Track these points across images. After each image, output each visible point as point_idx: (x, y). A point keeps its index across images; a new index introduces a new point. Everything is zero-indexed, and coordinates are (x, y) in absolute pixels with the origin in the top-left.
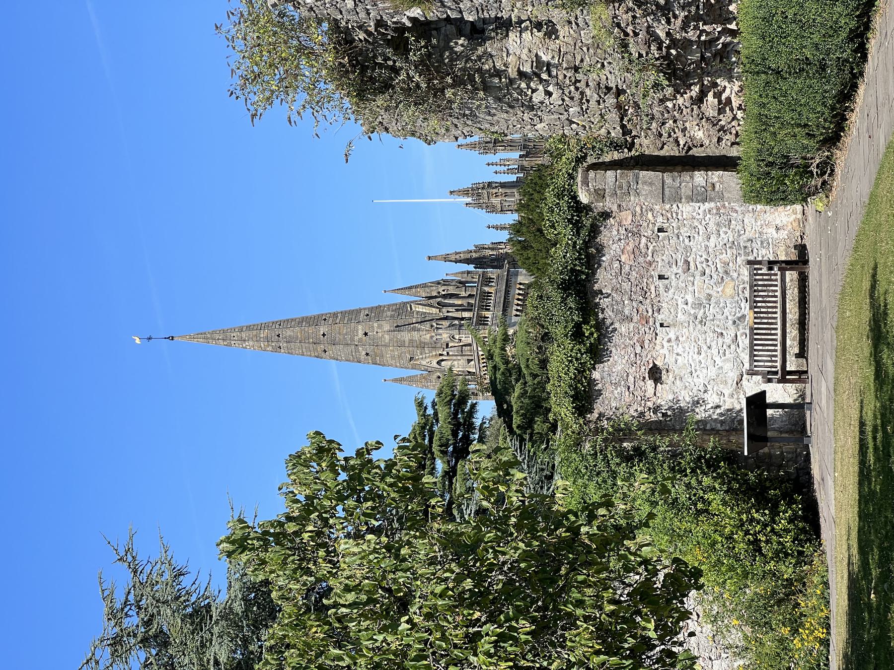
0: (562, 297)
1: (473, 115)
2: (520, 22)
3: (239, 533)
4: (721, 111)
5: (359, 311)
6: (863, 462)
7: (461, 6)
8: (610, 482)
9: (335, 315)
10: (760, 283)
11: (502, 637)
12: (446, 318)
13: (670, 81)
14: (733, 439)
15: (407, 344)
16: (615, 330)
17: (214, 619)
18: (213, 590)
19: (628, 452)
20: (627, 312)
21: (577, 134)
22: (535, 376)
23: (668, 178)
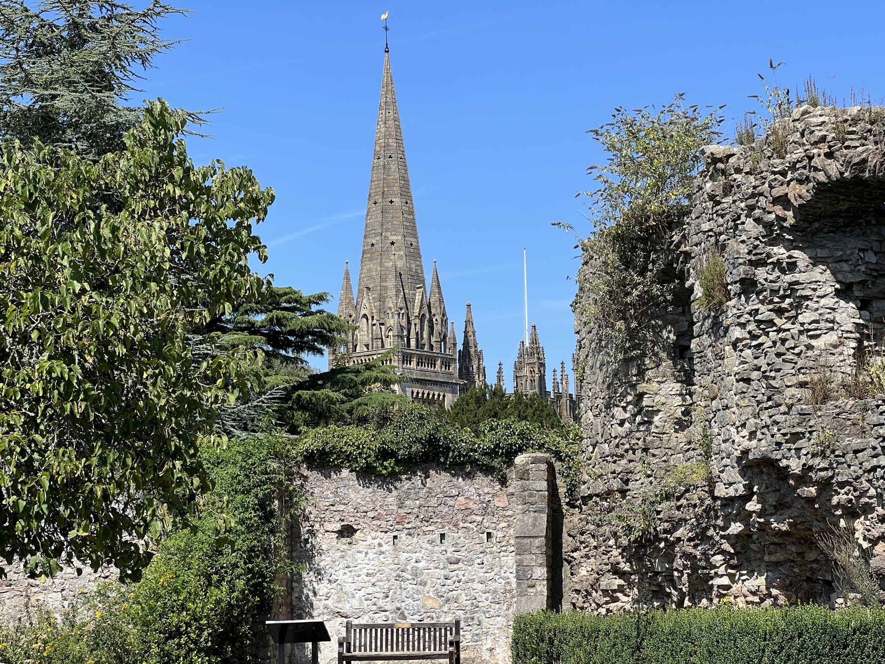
0: (421, 438)
1: (599, 349)
2: (691, 394)
3: (171, 121)
4: (605, 592)
5: (415, 236)
7: (705, 336)
8: (239, 487)
9: (411, 213)
10: (438, 634)
12: (409, 323)
13: (635, 542)
14: (283, 610)
15: (383, 284)
16: (390, 491)
17: (98, 94)
19: (269, 505)
20: (407, 503)
21: (583, 452)
22: (350, 412)
23: (540, 541)
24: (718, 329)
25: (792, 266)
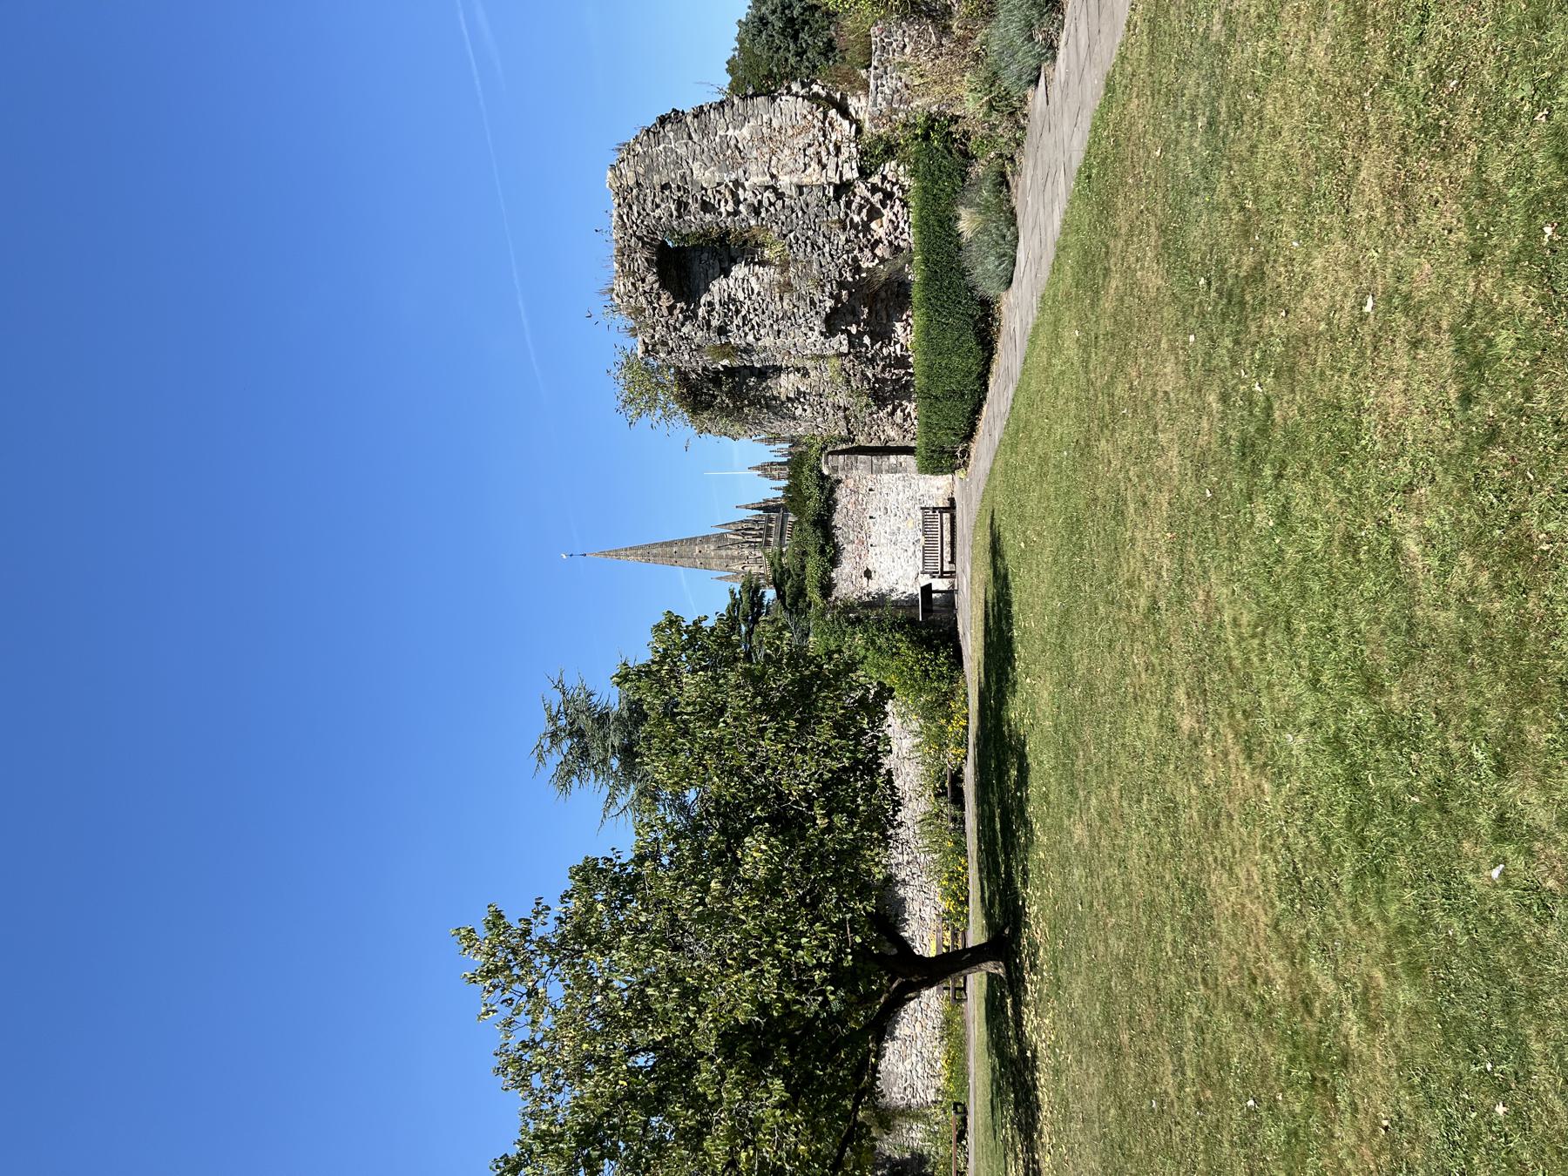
6: (986, 624)
11: (779, 730)
18: (611, 703)
24: (748, 350)
25: (710, 304)
